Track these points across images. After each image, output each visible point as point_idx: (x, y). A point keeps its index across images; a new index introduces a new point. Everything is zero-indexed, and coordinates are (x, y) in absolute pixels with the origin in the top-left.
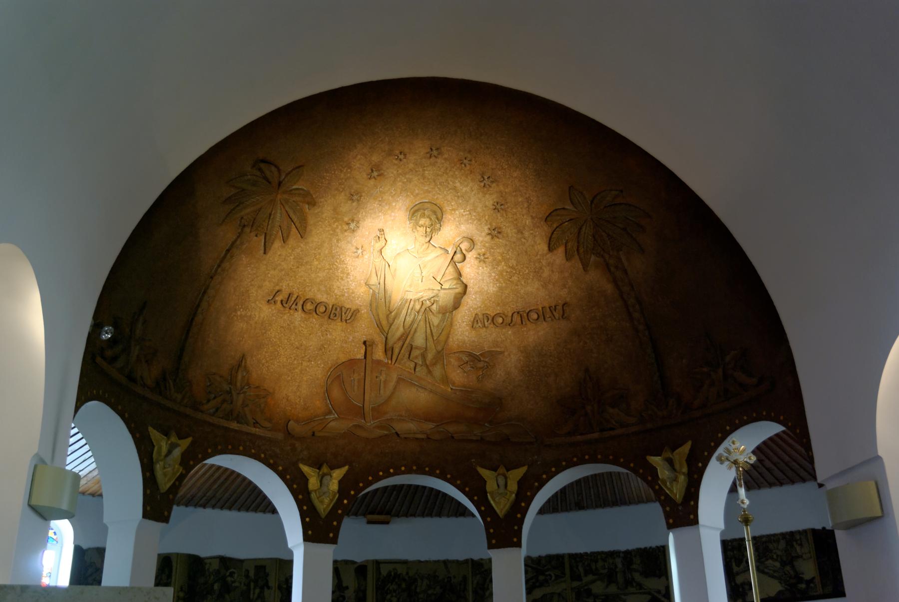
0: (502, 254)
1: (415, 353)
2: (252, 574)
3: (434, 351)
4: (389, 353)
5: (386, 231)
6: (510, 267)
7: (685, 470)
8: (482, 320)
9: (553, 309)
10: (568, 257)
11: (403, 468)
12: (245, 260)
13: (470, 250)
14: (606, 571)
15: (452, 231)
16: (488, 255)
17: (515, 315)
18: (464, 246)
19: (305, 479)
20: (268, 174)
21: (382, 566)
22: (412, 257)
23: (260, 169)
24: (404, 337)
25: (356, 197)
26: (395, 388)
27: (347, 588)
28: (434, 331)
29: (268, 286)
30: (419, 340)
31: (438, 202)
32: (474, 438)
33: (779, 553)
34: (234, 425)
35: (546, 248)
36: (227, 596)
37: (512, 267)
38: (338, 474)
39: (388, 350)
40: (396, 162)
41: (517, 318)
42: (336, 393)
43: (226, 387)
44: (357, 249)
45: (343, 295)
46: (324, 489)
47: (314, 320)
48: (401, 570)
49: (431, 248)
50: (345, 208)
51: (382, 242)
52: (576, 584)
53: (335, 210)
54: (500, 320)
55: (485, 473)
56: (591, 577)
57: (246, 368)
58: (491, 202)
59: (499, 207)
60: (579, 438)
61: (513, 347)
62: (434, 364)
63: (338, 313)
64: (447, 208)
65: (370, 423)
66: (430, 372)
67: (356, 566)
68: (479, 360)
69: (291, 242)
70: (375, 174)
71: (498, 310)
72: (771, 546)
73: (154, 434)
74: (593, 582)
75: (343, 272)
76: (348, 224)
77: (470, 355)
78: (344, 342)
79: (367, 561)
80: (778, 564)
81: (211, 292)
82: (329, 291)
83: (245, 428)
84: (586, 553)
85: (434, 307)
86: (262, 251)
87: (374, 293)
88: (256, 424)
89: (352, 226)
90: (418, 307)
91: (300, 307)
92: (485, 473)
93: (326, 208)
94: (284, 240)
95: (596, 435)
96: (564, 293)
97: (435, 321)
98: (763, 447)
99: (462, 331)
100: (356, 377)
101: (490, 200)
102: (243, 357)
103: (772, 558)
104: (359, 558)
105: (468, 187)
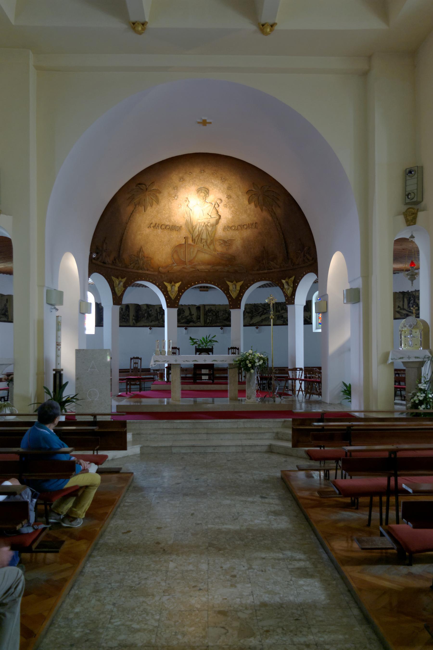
0: (232, 204)
1: (203, 241)
2: (158, 310)
3: (210, 240)
4: (194, 241)
7: (292, 286)
8: (227, 228)
9: (252, 224)
10: (256, 206)
12: (138, 215)
13: (221, 203)
15: (212, 198)
16: (227, 205)
17: (239, 227)
18: (219, 202)
19: (166, 287)
20: (142, 188)
22: (200, 208)
23: (139, 187)
24: (199, 235)
25: (176, 188)
26: (197, 254)
27: (193, 314)
28: (210, 233)
29: (147, 222)
30: (204, 236)
31: (207, 187)
34: (140, 271)
35: (248, 203)
37: (237, 209)
38: (178, 285)
39: (193, 240)
41: (239, 227)
42: (175, 256)
43: (136, 259)
46: (173, 290)
47: (166, 231)
48: (213, 308)
49: (206, 203)
50: (172, 192)
51: (188, 202)
52: (278, 313)
53: (168, 193)
54: (234, 228)
55: (229, 283)
57: (143, 252)
59: (229, 188)
60: (261, 272)
61: (239, 238)
62: (210, 244)
63: (174, 228)
64: (210, 189)
65: (188, 266)
66: (209, 248)
68: (227, 243)
69: (154, 206)
70: (182, 180)
71: (233, 224)
73: (114, 278)
75: (174, 214)
77: (223, 241)
78: (177, 238)
81: (127, 228)
82: (170, 221)
83: (144, 272)
85: (209, 224)
87: (187, 220)
88: (148, 270)
89: (176, 198)
90: (203, 225)
92: (229, 283)
93: (165, 193)
94: (151, 206)
95: (266, 271)
96: (255, 219)
97: (210, 229)
99: (220, 232)
100: (182, 250)
101: (226, 186)
102: (141, 247)
104: (198, 304)
105: (217, 182)
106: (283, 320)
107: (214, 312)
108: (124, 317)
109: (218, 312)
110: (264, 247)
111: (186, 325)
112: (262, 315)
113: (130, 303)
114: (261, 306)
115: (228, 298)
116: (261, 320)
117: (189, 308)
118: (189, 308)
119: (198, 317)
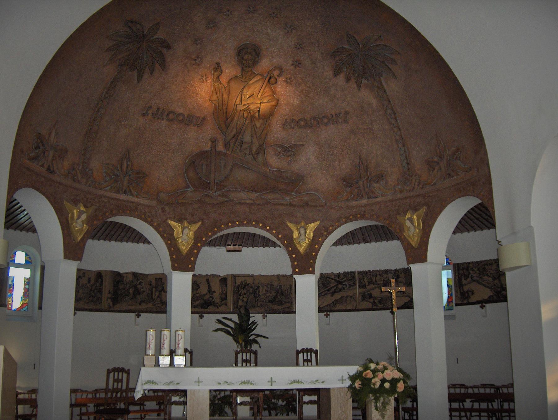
2: (153, 283)
5: (222, 63)
6: (307, 87)
11: (237, 223)
13: (279, 75)
14: (382, 282)
21: (236, 278)
26: (231, 170)
27: (215, 292)
32: (285, 203)
33: (492, 272)
36: (138, 296)
40: (225, 17)
44: (202, 76)
45: (194, 108)
48: (250, 281)
52: (362, 290)
56: (372, 286)
58: (293, 43)
66: (255, 159)
67: (220, 278)
72: (487, 267)
74: (373, 289)
76: (195, 60)
79: (227, 275)
80: (490, 279)
84: (369, 271)
86: (136, 81)
91: (165, 117)
94: (152, 72)
98: (472, 211)
103: (487, 275)
104: (222, 274)
106: (372, 300)
107: (251, 287)
108: (93, 294)
109: (258, 287)
110: (360, 158)
111: (203, 310)
112: (335, 292)
113: (104, 269)
114: (333, 277)
115: (290, 254)
116: (333, 301)
117: (208, 281)
118: (208, 281)
119: (224, 296)
